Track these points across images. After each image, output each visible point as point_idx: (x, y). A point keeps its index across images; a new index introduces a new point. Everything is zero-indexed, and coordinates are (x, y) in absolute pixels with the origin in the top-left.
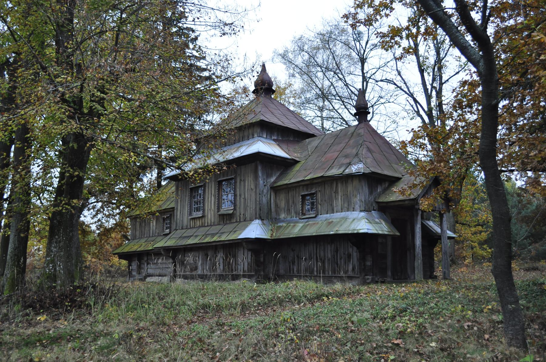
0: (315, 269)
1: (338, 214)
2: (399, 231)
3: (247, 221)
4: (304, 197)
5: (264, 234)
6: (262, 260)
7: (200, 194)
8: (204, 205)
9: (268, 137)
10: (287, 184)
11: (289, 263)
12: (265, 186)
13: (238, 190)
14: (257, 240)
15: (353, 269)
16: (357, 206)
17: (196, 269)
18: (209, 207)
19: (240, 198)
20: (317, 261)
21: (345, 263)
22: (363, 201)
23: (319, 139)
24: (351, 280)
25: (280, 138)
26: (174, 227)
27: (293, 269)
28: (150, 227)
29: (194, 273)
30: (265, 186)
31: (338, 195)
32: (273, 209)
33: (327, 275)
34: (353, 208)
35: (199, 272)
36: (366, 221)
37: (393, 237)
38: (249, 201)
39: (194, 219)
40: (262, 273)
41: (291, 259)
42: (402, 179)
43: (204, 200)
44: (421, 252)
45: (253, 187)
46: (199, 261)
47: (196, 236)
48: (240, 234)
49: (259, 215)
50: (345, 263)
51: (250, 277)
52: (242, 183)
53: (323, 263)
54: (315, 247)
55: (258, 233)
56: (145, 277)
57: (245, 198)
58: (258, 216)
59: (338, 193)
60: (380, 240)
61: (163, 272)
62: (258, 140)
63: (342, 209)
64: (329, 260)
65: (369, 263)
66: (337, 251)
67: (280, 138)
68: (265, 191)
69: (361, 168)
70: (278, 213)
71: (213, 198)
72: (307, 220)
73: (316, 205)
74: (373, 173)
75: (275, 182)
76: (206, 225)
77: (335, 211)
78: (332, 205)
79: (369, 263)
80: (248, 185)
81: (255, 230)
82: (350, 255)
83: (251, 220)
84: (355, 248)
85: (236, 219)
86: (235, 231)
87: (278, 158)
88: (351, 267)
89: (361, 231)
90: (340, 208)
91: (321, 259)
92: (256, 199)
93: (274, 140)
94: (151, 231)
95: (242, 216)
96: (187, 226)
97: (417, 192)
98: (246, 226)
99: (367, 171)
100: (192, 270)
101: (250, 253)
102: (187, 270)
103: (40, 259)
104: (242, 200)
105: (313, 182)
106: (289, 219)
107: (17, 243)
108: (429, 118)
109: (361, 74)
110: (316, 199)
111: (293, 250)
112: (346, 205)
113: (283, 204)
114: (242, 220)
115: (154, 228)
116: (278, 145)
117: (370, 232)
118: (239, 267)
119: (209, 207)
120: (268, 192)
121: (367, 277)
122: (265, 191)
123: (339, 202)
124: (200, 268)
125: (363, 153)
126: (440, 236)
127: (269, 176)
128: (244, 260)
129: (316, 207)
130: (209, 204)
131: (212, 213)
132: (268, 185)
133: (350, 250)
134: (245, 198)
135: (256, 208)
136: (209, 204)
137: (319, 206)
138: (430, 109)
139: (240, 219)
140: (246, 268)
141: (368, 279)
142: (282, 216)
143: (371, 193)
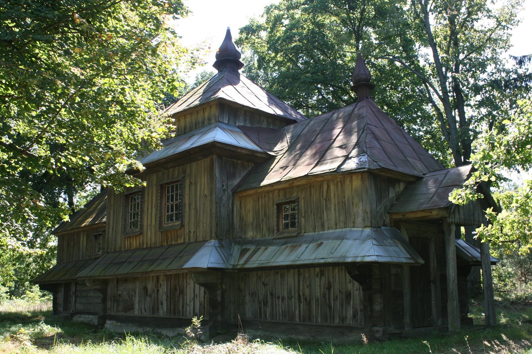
0: (297, 312)
1: (331, 231)
2: (424, 260)
5: (222, 262)
7: (138, 203)
8: (141, 218)
9: (231, 122)
11: (260, 303)
12: (224, 190)
14: (211, 270)
15: (355, 316)
16: (359, 220)
18: (149, 223)
19: (190, 209)
20: (300, 302)
21: (342, 305)
22: (369, 211)
23: (302, 125)
28: (79, 248)
29: (130, 314)
30: (224, 190)
31: (330, 204)
34: (354, 223)
35: (136, 312)
36: (375, 242)
37: (413, 268)
38: (202, 212)
40: (219, 318)
42: (424, 179)
43: (142, 211)
44: (456, 288)
45: (206, 192)
46: (135, 297)
47: (130, 263)
48: (187, 261)
49: (216, 233)
50: (342, 305)
52: (193, 187)
53: (309, 304)
54: (296, 277)
55: (212, 260)
56: (72, 315)
57: (196, 209)
58: (214, 235)
60: (394, 271)
62: (215, 127)
63: (336, 224)
64: (317, 300)
65: (377, 307)
68: (225, 198)
69: (366, 162)
71: (154, 209)
72: (285, 240)
73: (298, 218)
76: (145, 246)
77: (326, 226)
78: (321, 218)
79: (377, 307)
80: (200, 190)
81: (206, 258)
82: (350, 293)
84: (356, 284)
85: (185, 239)
86: (181, 257)
87: (243, 151)
88: (350, 313)
89: (367, 259)
90: (333, 222)
91: (305, 299)
92: (211, 210)
93: (239, 127)
94: (81, 253)
95: (192, 234)
96: (121, 248)
99: (374, 166)
101: (202, 289)
104: (193, 212)
108: (444, 105)
110: (298, 209)
112: (342, 218)
114: (192, 240)
115: (85, 250)
116: (245, 134)
117: (381, 260)
118: (188, 308)
119: (149, 223)
120: (228, 200)
121: (375, 328)
122: (225, 198)
123: (332, 215)
124: (137, 306)
125: (367, 140)
126: (480, 262)
127: (231, 176)
129: (298, 222)
130: (149, 217)
131: (153, 230)
132: (229, 190)
134: (196, 209)
135: (211, 223)
136: (149, 217)
137: (303, 220)
138: (445, 92)
139: (189, 239)
141: (377, 331)
142: (250, 234)
143: (379, 199)
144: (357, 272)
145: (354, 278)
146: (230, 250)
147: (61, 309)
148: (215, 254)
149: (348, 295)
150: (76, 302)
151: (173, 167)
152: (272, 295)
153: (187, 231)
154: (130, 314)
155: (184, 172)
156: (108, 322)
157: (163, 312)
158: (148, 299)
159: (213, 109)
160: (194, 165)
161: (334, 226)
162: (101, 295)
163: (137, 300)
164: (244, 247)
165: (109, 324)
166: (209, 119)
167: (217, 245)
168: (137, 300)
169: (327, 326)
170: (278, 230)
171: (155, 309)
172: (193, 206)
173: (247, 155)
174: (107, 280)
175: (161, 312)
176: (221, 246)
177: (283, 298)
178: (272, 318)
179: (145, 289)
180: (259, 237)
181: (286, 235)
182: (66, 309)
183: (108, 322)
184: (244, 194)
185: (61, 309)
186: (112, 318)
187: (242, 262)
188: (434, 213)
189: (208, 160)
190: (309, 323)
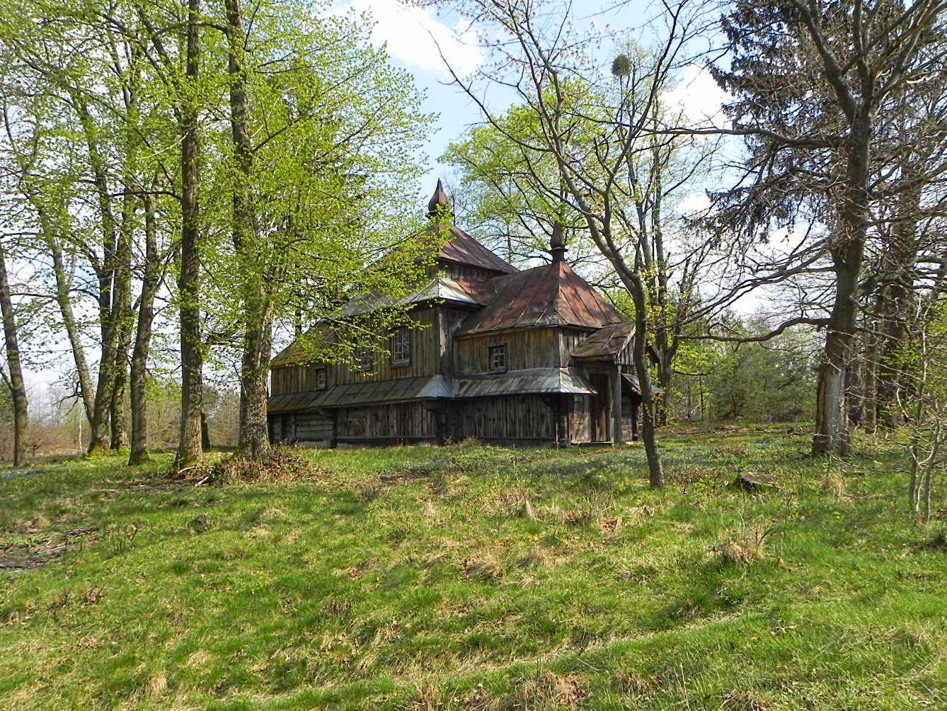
2: (597, 390)
3: (426, 378)
6: (444, 421)
13: (414, 340)
14: (440, 399)
17: (364, 431)
26: (332, 381)
32: (456, 363)
35: (368, 435)
37: (591, 396)
41: (476, 420)
48: (419, 392)
51: (430, 440)
53: (514, 424)
61: (320, 436)
66: (529, 411)
70: (461, 368)
81: (434, 389)
83: (430, 376)
84: (549, 408)
90: (532, 362)
98: (425, 383)
100: (356, 434)
102: (350, 433)
104: (420, 352)
105: (501, 333)
106: (474, 373)
107: (466, 443)
109: (97, 292)
111: (479, 410)
112: (539, 360)
113: (466, 357)
123: (531, 357)
124: (368, 430)
128: (422, 422)
133: (544, 410)
140: (425, 431)
145: (547, 404)
149: (543, 416)
158: (379, 423)
171: (386, 431)
176: (445, 379)
179: (376, 415)
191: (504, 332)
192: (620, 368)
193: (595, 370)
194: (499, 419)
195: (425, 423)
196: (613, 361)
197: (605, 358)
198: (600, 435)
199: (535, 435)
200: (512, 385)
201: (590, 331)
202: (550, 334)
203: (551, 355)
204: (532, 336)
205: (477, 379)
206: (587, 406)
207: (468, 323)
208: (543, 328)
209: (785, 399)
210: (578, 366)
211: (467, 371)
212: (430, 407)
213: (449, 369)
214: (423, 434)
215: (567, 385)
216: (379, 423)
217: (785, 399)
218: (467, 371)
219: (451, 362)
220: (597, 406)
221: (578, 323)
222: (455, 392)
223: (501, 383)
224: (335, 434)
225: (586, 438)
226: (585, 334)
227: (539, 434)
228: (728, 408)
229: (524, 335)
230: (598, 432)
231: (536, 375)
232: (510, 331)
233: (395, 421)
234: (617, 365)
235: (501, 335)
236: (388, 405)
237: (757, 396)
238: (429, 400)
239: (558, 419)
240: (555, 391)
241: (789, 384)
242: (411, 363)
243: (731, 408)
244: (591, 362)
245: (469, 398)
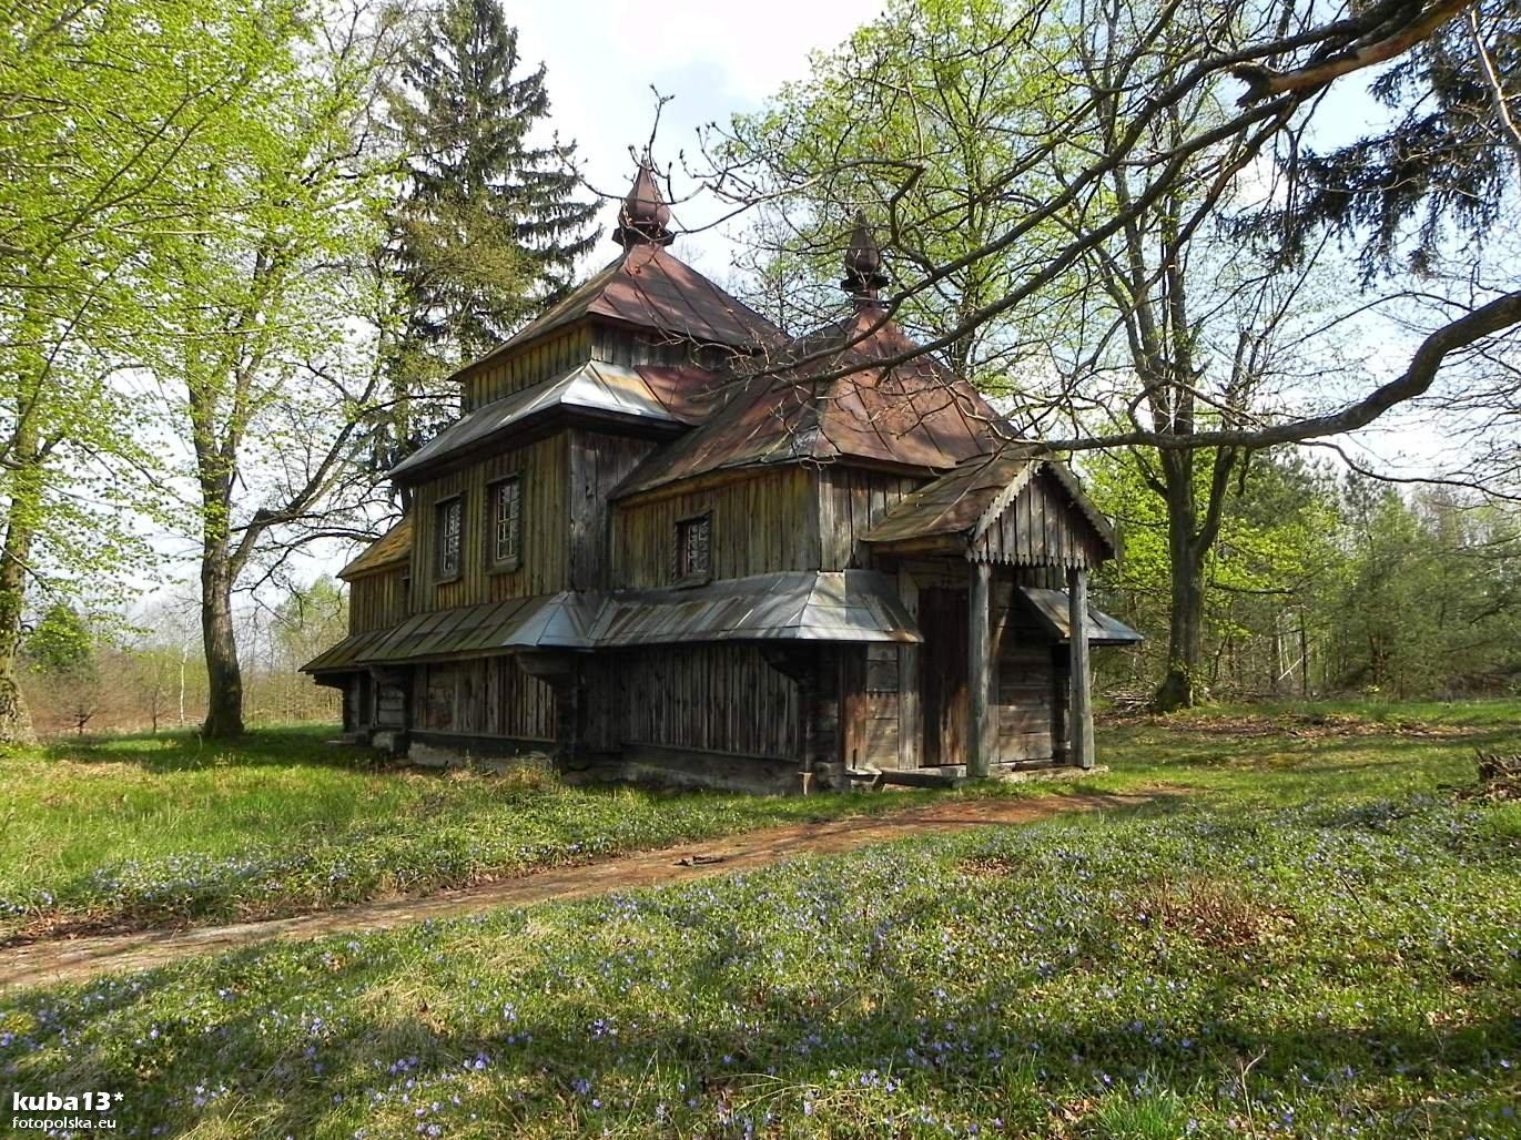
1: (758, 577)
4: (683, 527)
10: (694, 477)
24: (770, 773)
25: (661, 364)
27: (659, 730)
33: (729, 752)
34: (793, 562)
35: (454, 729)
39: (444, 585)
40: (574, 740)
57: (541, 533)
59: (758, 516)
67: (661, 364)
70: (628, 575)
72: (686, 593)
74: (847, 456)
75: (620, 487)
81: (546, 627)
88: (783, 735)
90: (762, 560)
91: (718, 706)
95: (535, 581)
97: (28, 762)
103: (212, 912)
104: (537, 537)
112: (777, 553)
123: (758, 547)
127: (604, 467)
128: (538, 704)
134: (541, 533)
144: (781, 657)
145: (779, 667)
146: (596, 612)
147: (356, 720)
148: (561, 617)
149: (781, 701)
150: (378, 709)
151: (509, 451)
152: (668, 694)
153: (528, 575)
154: (444, 732)
155: (525, 461)
156: (414, 746)
157: (492, 729)
158: (472, 701)
159: (583, 332)
160: (539, 445)
161: (762, 567)
162: (401, 695)
163: (455, 707)
164: (625, 605)
165: (416, 751)
166: (496, 393)
167: (570, 601)
168: (455, 707)
169: (749, 758)
170: (680, 572)
171: (482, 723)
172: (538, 528)
173: (634, 425)
174: (413, 666)
175: (490, 726)
176: (580, 602)
177: (685, 703)
178: (669, 742)
179: (468, 683)
180: (651, 587)
181: (689, 583)
182: (364, 721)
183: (414, 746)
184: (628, 503)
185: (356, 720)
186: (420, 738)
187: (609, 635)
188: (941, 543)
189: (560, 437)
190: (720, 752)
191: (706, 483)
192: (984, 572)
193: (924, 578)
194: (695, 704)
195: (542, 705)
196: (962, 557)
197: (941, 543)
198: (954, 746)
199: (763, 749)
200: (705, 619)
201: (919, 476)
202: (801, 484)
203: (801, 538)
204: (763, 487)
205: (651, 599)
206: (909, 670)
207: (652, 465)
208: (783, 469)
209: (1484, 643)
210: (879, 568)
211: (639, 581)
212: (539, 667)
213: (594, 578)
214: (539, 733)
215: (821, 614)
216: (472, 701)
217: (1484, 643)
218: (639, 581)
219: (604, 561)
220: (939, 678)
221: (884, 457)
222: (603, 631)
223: (690, 611)
224: (409, 722)
225: (907, 760)
226: (906, 485)
227: (773, 746)
228: (1360, 660)
229: (747, 488)
230: (947, 739)
231: (763, 592)
232: (691, 486)
233: (496, 700)
234: (975, 566)
235: (701, 491)
236: (487, 659)
237: (1422, 640)
238: (546, 652)
239: (812, 709)
240: (786, 634)
241: (1494, 612)
242: (521, 565)
243: (1366, 663)
244: (925, 556)
245: (619, 648)
